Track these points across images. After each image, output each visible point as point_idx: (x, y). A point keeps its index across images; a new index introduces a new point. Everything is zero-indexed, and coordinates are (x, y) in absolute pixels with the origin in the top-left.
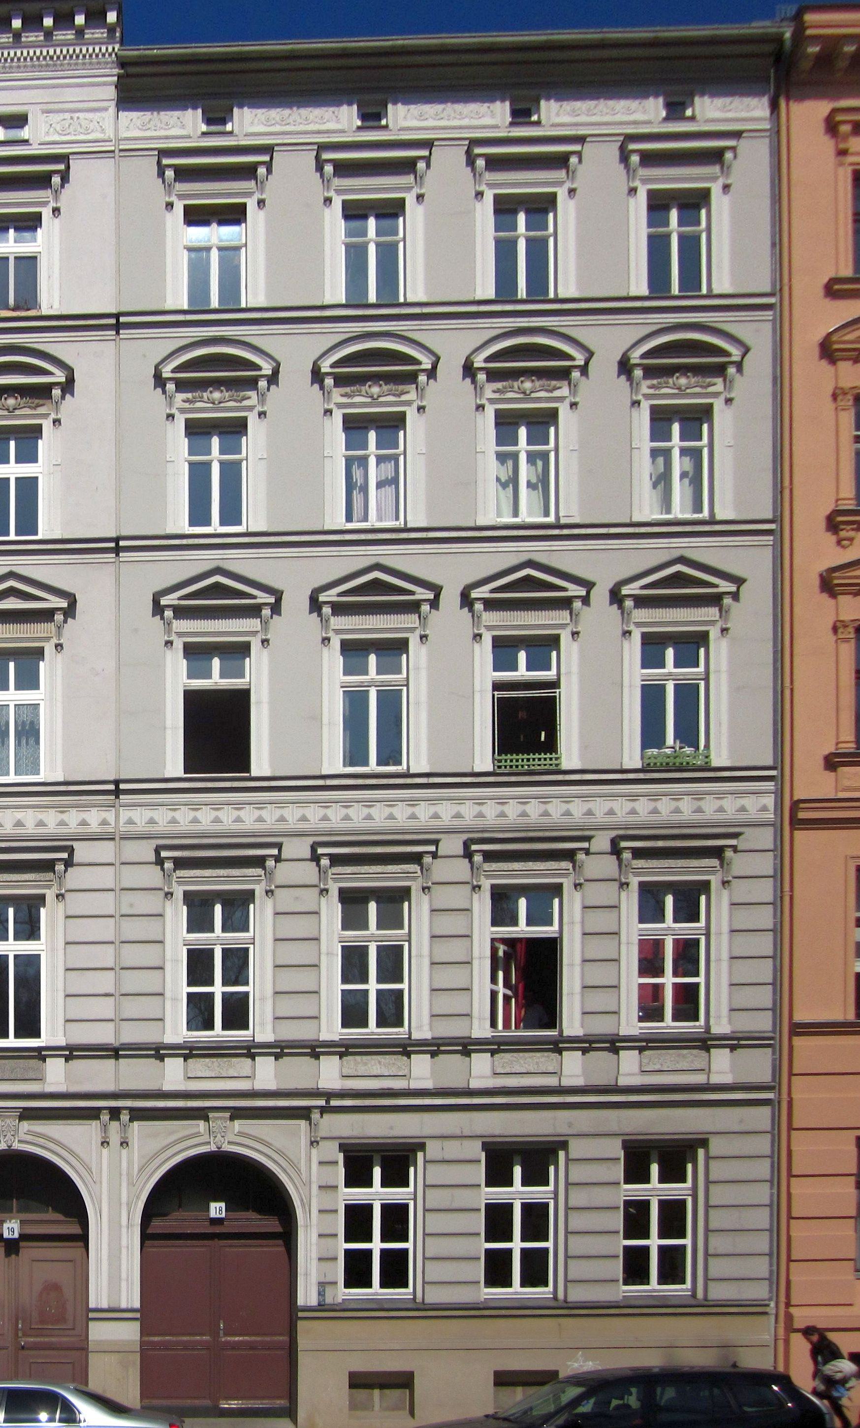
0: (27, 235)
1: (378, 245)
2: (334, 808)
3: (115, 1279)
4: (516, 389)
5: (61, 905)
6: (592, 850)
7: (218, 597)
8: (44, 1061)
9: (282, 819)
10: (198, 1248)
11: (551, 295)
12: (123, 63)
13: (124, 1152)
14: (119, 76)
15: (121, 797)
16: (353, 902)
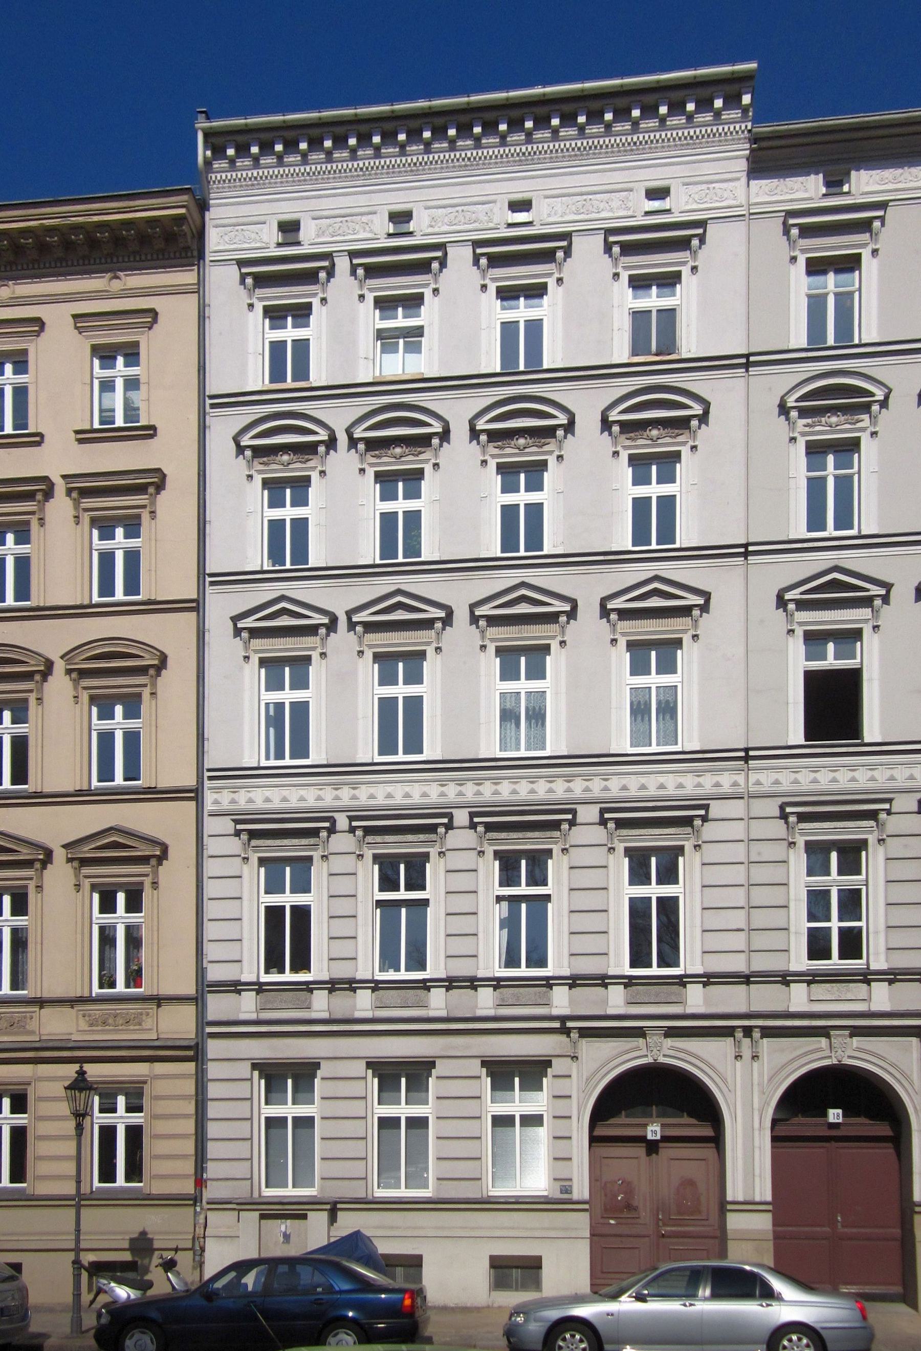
0: (535, 301)
1: (836, 294)
2: (784, 774)
3: (749, 1174)
4: (823, 423)
5: (565, 858)
6: (893, 810)
7: (836, 591)
8: (685, 987)
9: (892, 778)
10: (818, 1151)
11: (856, 341)
12: (755, 139)
13: (755, 1065)
14: (752, 151)
15: (750, 762)
16: (817, 854)
